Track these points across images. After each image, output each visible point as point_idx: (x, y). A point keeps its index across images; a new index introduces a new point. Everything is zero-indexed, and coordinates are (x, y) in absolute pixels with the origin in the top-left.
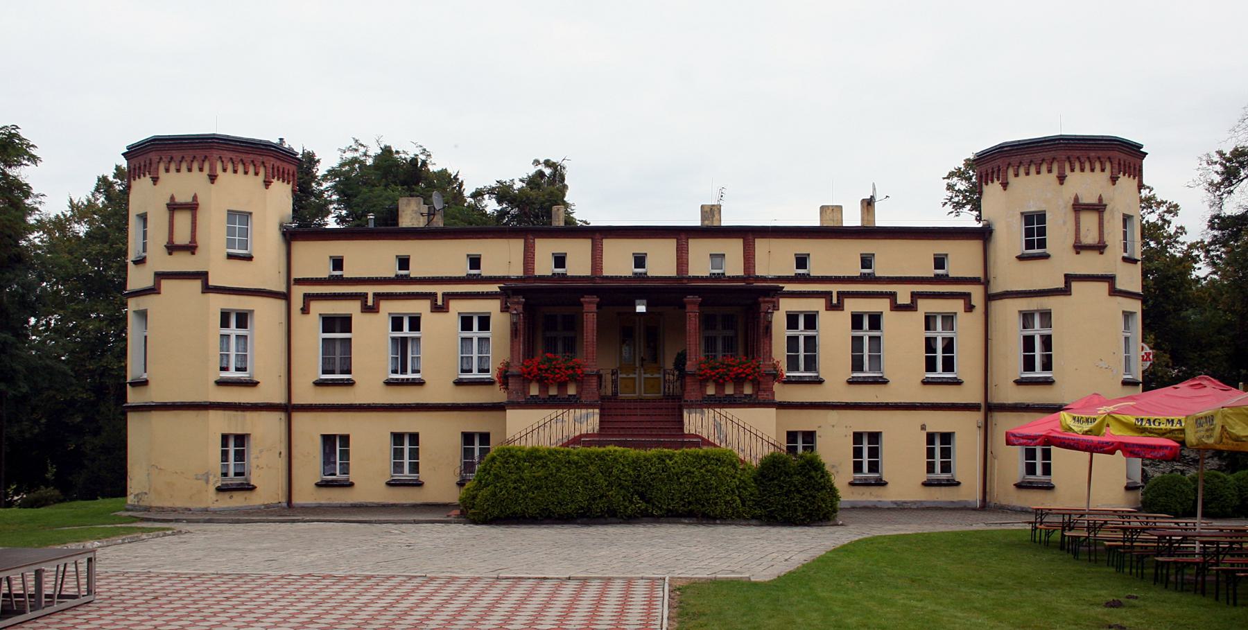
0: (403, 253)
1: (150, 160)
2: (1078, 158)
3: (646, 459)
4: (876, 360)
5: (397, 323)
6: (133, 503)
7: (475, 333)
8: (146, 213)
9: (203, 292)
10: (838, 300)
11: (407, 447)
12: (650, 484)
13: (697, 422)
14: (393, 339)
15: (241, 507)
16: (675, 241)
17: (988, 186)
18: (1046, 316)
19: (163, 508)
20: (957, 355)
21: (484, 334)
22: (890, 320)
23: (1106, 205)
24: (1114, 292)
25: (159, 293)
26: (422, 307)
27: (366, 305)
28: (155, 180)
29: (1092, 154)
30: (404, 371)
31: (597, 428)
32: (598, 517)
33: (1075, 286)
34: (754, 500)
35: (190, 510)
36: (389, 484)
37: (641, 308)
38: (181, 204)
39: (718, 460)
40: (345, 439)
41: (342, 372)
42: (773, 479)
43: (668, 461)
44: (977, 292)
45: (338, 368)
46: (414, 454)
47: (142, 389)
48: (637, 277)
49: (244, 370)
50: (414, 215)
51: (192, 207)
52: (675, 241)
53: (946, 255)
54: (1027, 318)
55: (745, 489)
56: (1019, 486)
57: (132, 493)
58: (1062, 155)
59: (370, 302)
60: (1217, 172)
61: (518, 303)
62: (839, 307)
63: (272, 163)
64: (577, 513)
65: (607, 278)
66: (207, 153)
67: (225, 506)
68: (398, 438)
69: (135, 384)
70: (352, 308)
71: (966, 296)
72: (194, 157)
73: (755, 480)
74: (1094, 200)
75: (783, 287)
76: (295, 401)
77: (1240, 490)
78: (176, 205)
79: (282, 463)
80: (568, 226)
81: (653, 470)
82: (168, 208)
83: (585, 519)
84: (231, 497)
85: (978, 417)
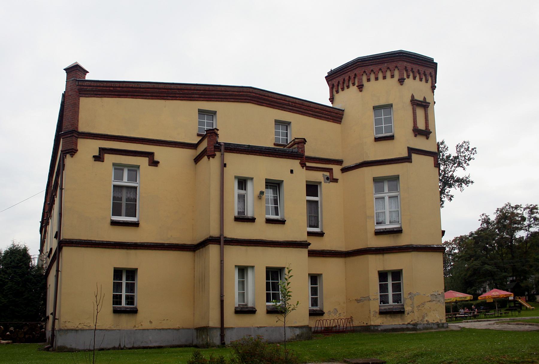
11: (390, 282)
17: (339, 93)
63: (423, 70)
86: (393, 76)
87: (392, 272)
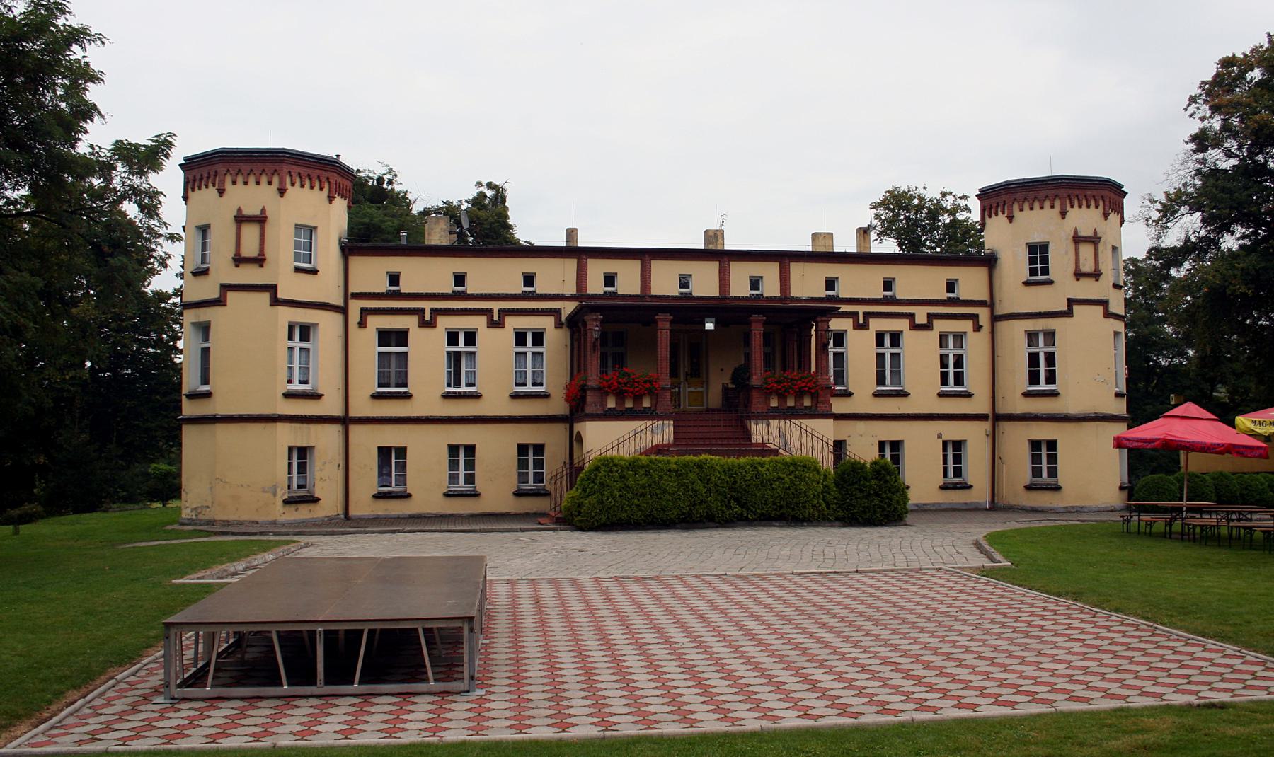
0: (460, 270)
1: (216, 172)
2: (1077, 196)
3: (741, 467)
4: (896, 374)
5: (453, 338)
7: (529, 348)
9: (271, 305)
10: (864, 320)
11: (462, 458)
12: (745, 490)
13: (762, 432)
14: (449, 353)
16: (717, 263)
18: (1050, 336)
19: (228, 521)
20: (967, 370)
21: (538, 349)
22: (909, 338)
23: (1100, 238)
24: (1108, 314)
25: (225, 305)
26: (478, 323)
27: (493, 320)
28: (221, 192)
29: (1089, 193)
30: (458, 384)
31: (672, 439)
32: (698, 521)
33: (1076, 308)
34: (837, 504)
35: (257, 523)
36: (447, 495)
37: (709, 326)
39: (804, 466)
40: (402, 452)
41: (397, 386)
42: (853, 484)
43: (760, 468)
44: (984, 314)
45: (393, 380)
46: (470, 465)
48: (683, 297)
50: (443, 233)
51: (260, 220)
52: (717, 263)
53: (894, 279)
54: (1032, 337)
55: (829, 493)
56: (1029, 488)
58: (1064, 192)
59: (427, 318)
60: (1157, 210)
61: (596, 320)
62: (929, 327)
64: (679, 518)
65: (656, 296)
66: (277, 166)
67: (292, 518)
68: (454, 450)
69: (193, 396)
70: (409, 322)
71: (974, 317)
72: (264, 170)
73: (837, 485)
74: (1090, 234)
75: (840, 308)
76: (352, 414)
77: (1216, 488)
78: (244, 217)
79: (339, 475)
80: (462, 244)
81: (748, 477)
83: (683, 524)
84: (297, 509)
85: (986, 426)
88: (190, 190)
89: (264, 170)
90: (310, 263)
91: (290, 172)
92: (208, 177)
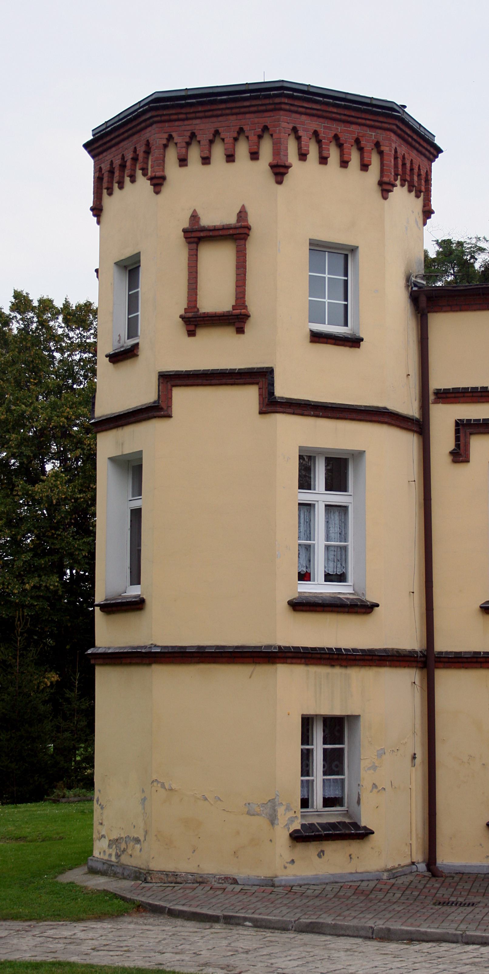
1: (148, 144)
6: (106, 857)
8: (138, 255)
15: (341, 876)
19: (175, 875)
35: (235, 882)
38: (215, 229)
47: (131, 618)
49: (341, 578)
57: (103, 836)
63: (394, 146)
66: (267, 119)
72: (241, 131)
78: (204, 229)
82: (186, 238)
84: (321, 854)
86: (231, 159)
87: (324, 718)
88: (105, 191)
89: (241, 131)
90: (346, 324)
91: (295, 130)
92: (135, 159)
